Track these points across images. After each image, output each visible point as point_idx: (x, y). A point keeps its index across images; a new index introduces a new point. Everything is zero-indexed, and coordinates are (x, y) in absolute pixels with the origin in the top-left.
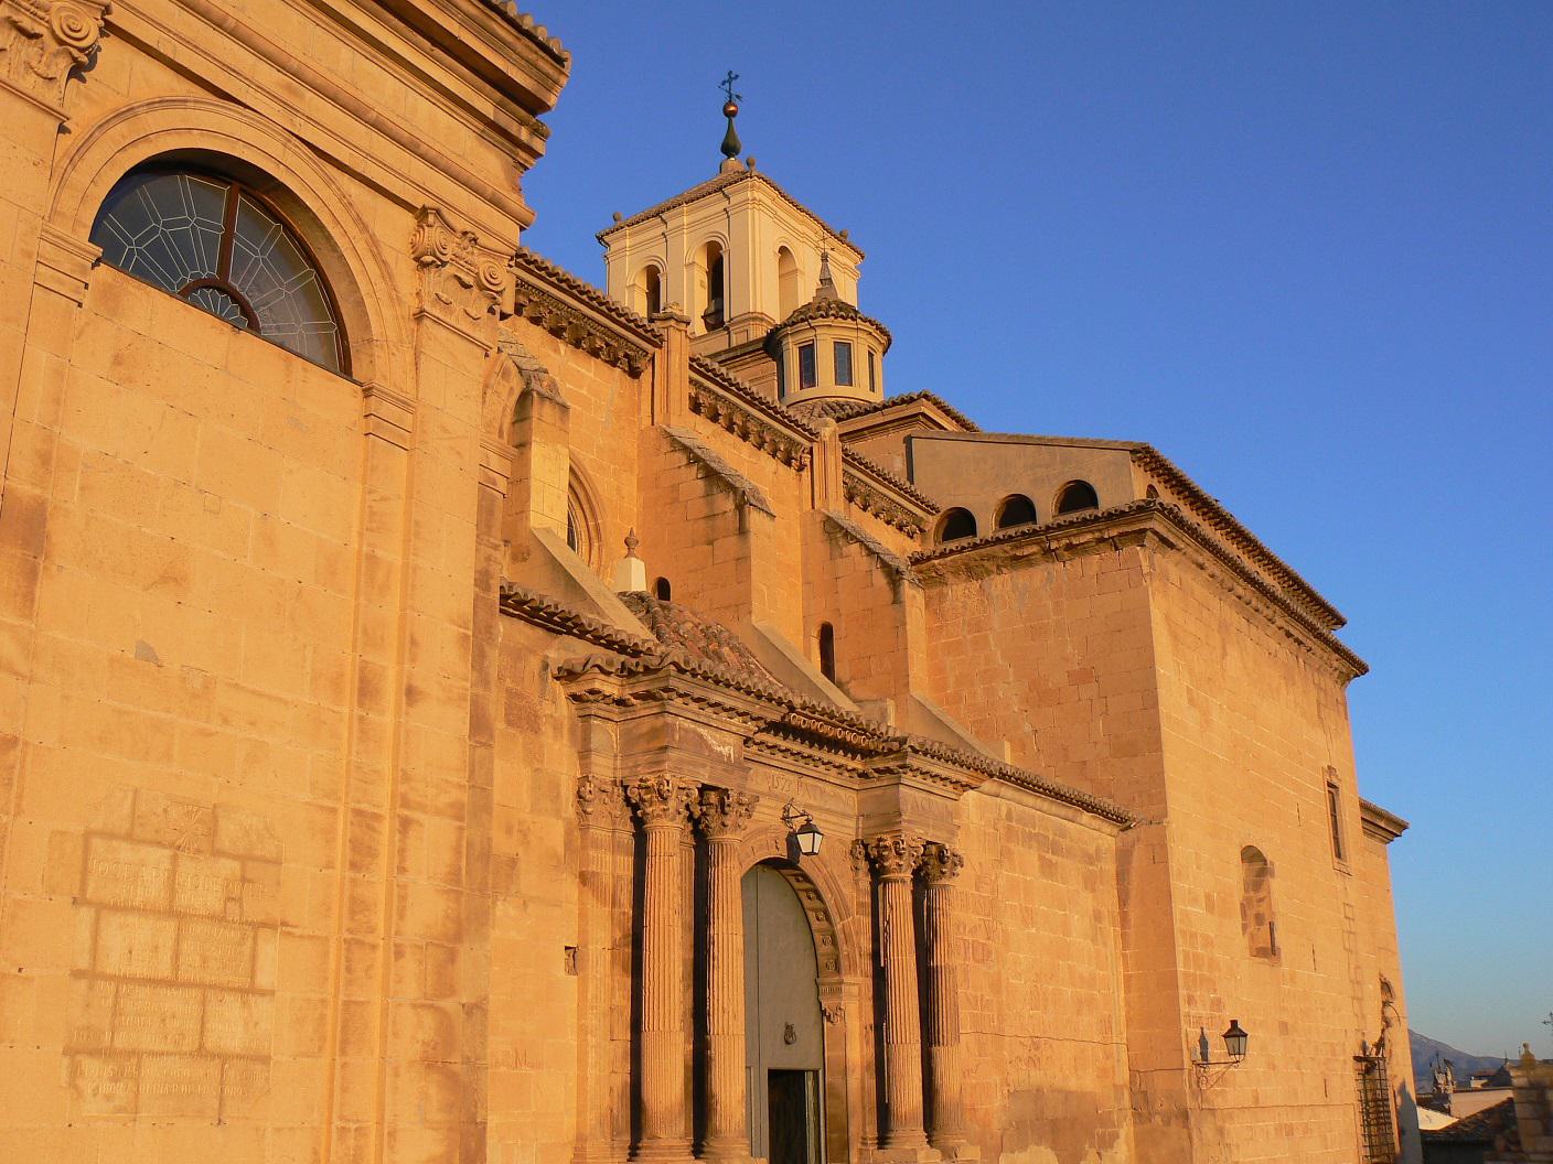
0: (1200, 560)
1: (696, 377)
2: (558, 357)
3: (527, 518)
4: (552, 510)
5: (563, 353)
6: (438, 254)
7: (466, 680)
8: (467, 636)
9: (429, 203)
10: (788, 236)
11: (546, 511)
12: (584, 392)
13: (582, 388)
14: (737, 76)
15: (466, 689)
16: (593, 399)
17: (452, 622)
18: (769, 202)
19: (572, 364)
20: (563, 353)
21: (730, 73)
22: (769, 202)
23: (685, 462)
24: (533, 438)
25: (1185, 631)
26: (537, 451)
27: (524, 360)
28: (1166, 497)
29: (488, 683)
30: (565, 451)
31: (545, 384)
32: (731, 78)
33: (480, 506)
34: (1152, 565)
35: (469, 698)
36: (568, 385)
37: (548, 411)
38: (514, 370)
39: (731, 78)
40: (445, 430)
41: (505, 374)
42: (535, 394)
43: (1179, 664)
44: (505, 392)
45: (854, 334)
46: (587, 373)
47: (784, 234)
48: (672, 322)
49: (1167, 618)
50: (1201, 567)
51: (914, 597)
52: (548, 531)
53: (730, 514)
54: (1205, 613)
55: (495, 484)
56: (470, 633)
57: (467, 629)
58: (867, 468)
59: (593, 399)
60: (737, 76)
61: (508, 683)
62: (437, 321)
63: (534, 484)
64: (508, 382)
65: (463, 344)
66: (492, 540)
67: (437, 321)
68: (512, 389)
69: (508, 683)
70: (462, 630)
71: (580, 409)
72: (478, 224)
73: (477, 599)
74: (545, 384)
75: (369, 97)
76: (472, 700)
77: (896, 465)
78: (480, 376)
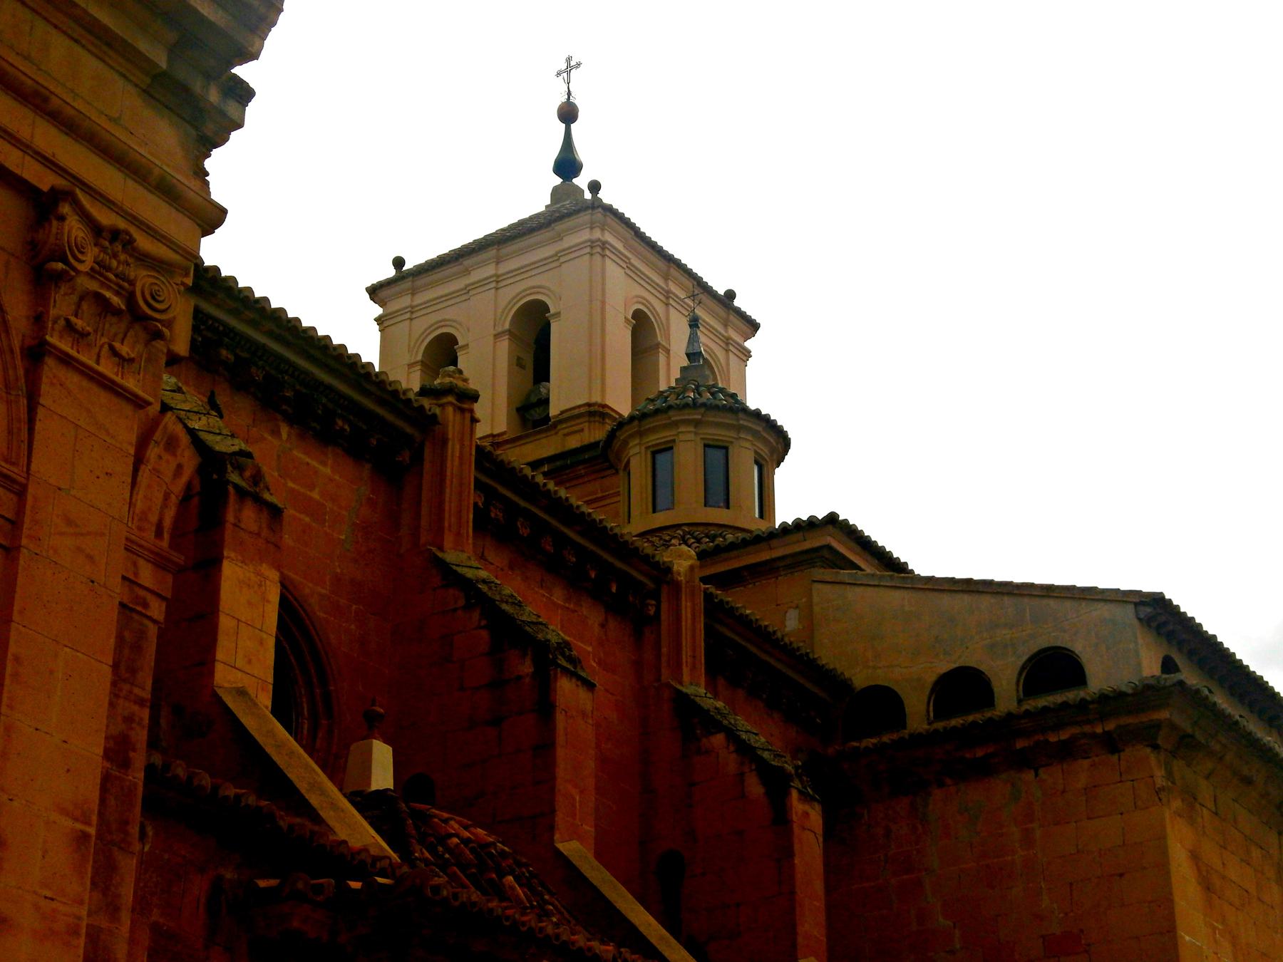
0: (1245, 771)
1: (484, 479)
2: (276, 442)
3: (211, 673)
4: (250, 662)
5: (284, 436)
6: (72, 260)
7: (81, 902)
8: (86, 836)
9: (61, 182)
10: (646, 295)
11: (240, 663)
12: (315, 495)
13: (312, 487)
14: (578, 65)
15: (79, 918)
16: (329, 505)
17: (64, 811)
18: (619, 246)
19: (298, 454)
20: (284, 436)
21: (569, 59)
22: (619, 246)
23: (461, 602)
24: (225, 554)
25: (1224, 878)
26: (232, 573)
27: (219, 438)
28: (1190, 676)
29: (117, 909)
30: (274, 575)
31: (247, 474)
32: (570, 67)
33: (120, 638)
34: (1169, 775)
35: (84, 931)
36: (291, 484)
37: (250, 516)
38: (185, 439)
39: (570, 67)
40: (69, 522)
41: (171, 444)
42: (231, 488)
43: (1214, 928)
44: (168, 469)
45: (732, 434)
46: (321, 468)
47: (639, 291)
48: (451, 399)
49: (1195, 856)
50: (1248, 781)
51: (806, 815)
52: (241, 692)
53: (527, 680)
54: (1256, 853)
55: (146, 605)
56: (92, 831)
57: (88, 823)
58: (747, 625)
59: (329, 505)
60: (578, 65)
61: (156, 916)
62: (66, 360)
63: (225, 622)
64: (174, 455)
65: (103, 397)
66: (136, 691)
67: (66, 360)
68: (180, 467)
69: (156, 916)
70: (79, 826)
71: (307, 519)
72: (134, 219)
73: (106, 779)
74: (247, 474)
75: (425, 310)
76: (88, 935)
77: (788, 623)
78: (130, 444)
